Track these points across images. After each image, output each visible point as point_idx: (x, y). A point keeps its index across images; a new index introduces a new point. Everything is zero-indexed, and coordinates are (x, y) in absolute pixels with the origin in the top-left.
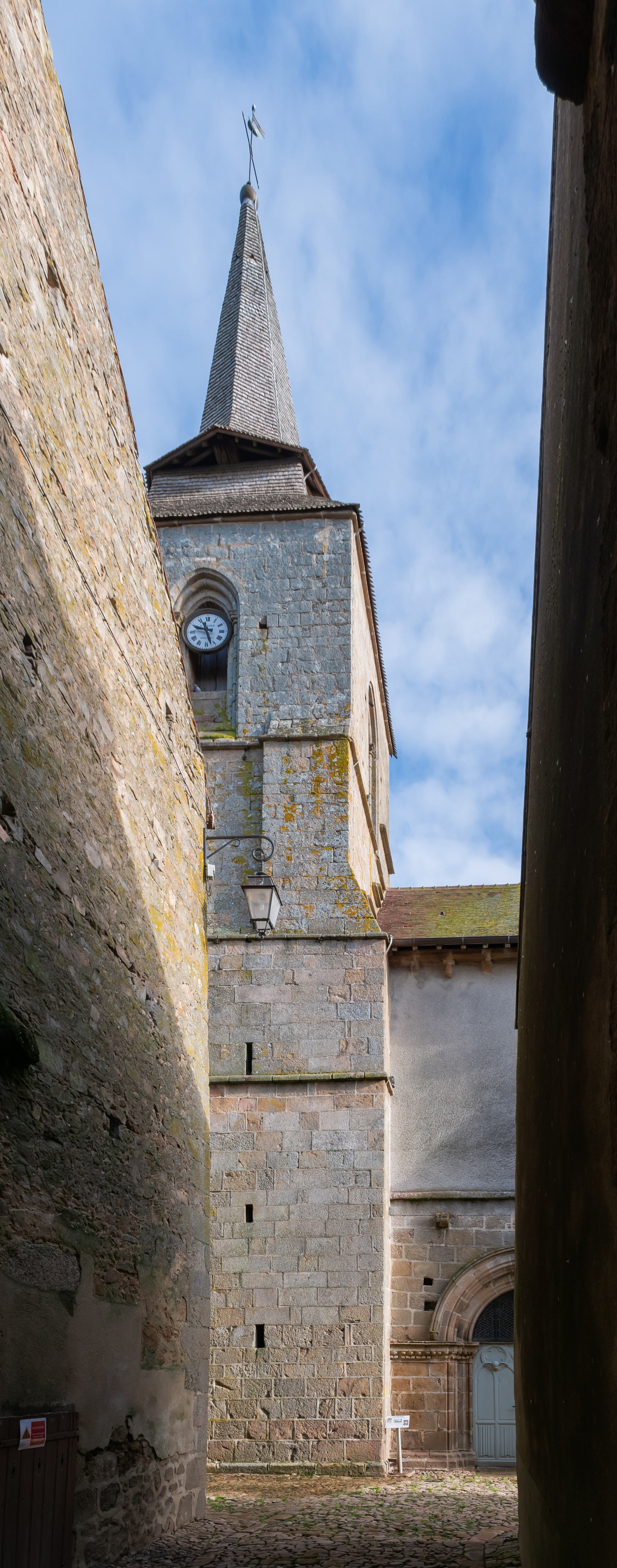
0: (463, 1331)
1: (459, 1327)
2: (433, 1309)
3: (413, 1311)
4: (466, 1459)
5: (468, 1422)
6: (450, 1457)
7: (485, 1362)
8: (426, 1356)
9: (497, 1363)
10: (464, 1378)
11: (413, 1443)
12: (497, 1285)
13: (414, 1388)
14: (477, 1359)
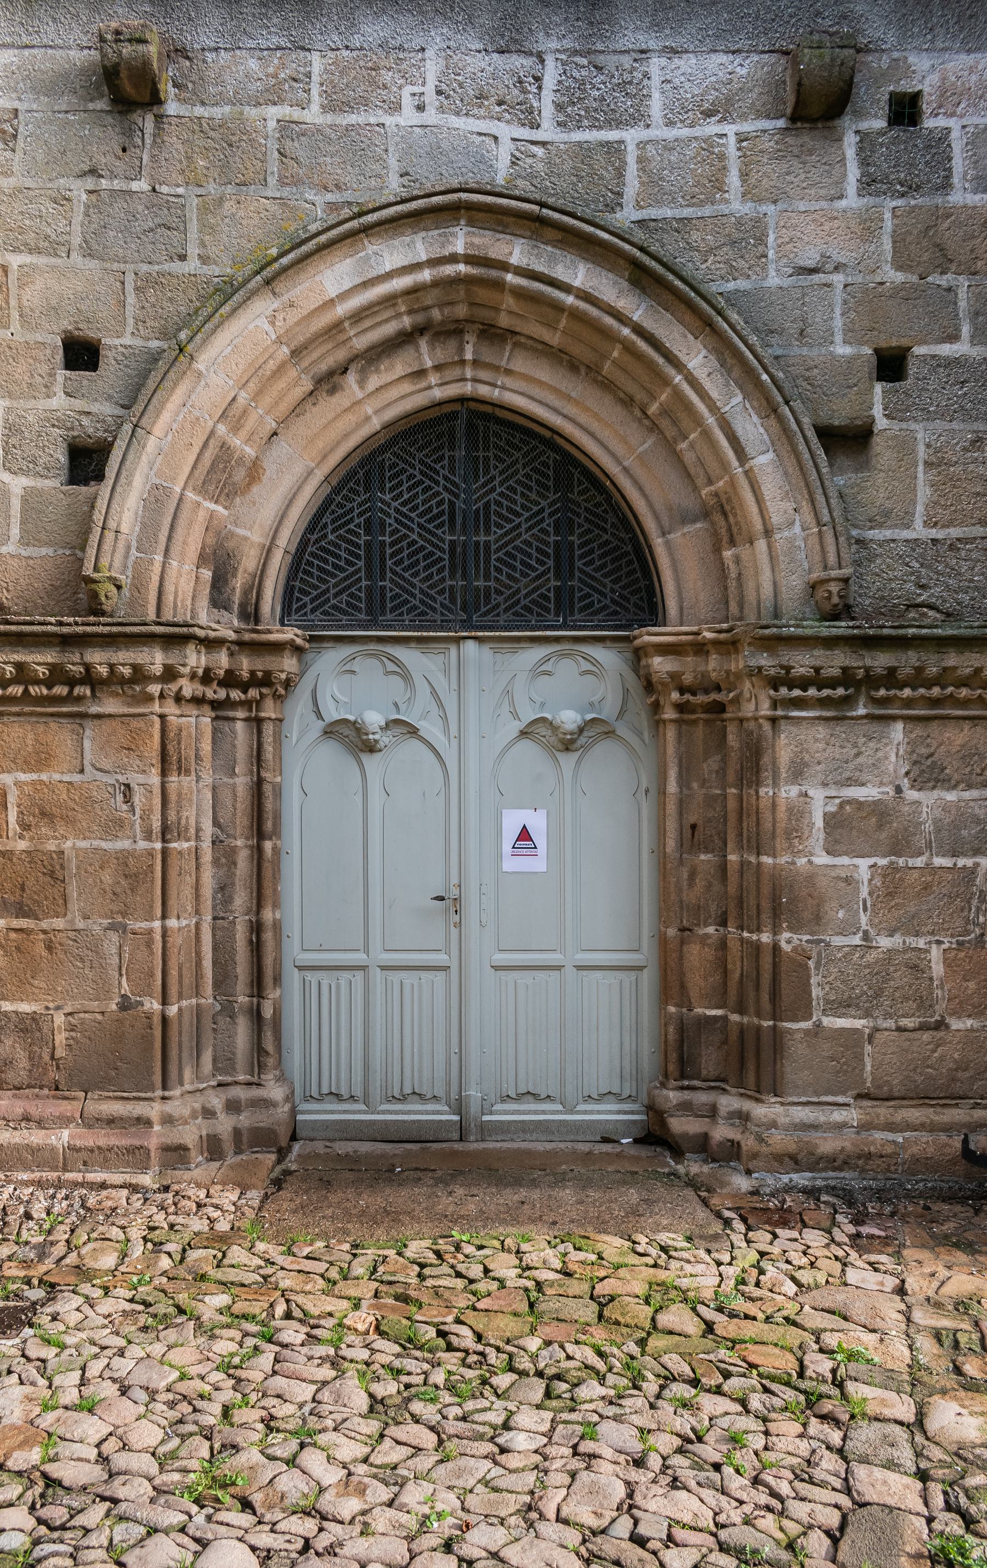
0: (238, 583)
1: (219, 562)
2: (99, 477)
3: (18, 484)
4: (245, 1120)
5: (254, 964)
6: (168, 1120)
7: (332, 713)
8: (72, 682)
9: (374, 719)
10: (242, 782)
11: (22, 1062)
12: (374, 382)
13: (25, 826)
14: (299, 706)
